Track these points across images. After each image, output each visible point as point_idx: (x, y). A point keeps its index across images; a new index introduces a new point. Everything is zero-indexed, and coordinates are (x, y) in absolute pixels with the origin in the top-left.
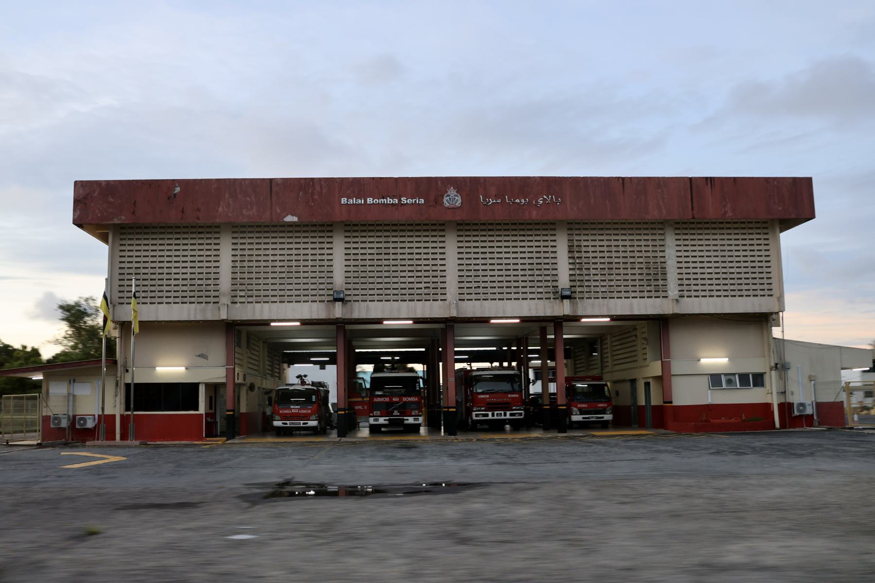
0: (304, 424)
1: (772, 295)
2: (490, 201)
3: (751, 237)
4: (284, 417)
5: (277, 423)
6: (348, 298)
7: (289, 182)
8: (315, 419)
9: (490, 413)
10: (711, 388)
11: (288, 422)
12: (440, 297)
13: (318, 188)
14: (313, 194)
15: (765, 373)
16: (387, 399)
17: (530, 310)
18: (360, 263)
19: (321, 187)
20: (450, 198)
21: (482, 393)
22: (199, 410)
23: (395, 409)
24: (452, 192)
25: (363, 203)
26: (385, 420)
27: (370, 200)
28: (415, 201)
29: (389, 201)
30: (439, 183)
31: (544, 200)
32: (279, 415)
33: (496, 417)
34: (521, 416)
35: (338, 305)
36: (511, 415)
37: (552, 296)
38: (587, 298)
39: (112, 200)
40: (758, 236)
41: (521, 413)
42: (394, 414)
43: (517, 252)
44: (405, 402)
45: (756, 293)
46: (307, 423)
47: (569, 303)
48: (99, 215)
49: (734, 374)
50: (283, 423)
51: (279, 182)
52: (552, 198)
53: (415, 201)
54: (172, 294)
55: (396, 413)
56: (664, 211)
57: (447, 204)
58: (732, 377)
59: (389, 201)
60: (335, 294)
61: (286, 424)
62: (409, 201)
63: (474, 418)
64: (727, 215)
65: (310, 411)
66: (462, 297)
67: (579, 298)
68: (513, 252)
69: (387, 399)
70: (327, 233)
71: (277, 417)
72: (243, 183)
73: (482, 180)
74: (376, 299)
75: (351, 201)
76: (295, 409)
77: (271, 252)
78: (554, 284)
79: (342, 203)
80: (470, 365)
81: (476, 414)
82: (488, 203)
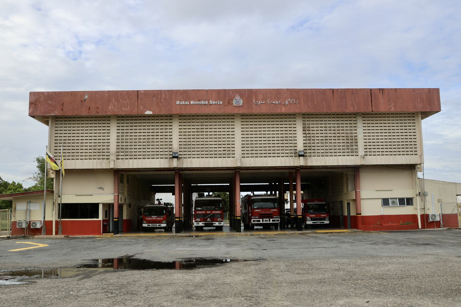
0: (159, 225)
4: (148, 222)
5: (145, 225)
7: (147, 93)
9: (261, 220)
11: (150, 224)
13: (164, 96)
14: (161, 99)
15: (413, 198)
16: (204, 212)
17: (281, 163)
19: (165, 94)
20: (236, 101)
24: (238, 98)
25: (188, 104)
26: (202, 224)
27: (192, 102)
28: (217, 103)
32: (146, 220)
33: (264, 222)
34: (279, 221)
35: (175, 160)
36: (273, 221)
38: (313, 156)
39: (50, 102)
41: (279, 220)
42: (208, 220)
44: (214, 214)
47: (303, 159)
49: (396, 198)
50: (148, 225)
51: (142, 92)
55: (209, 220)
56: (356, 108)
58: (395, 200)
61: (150, 225)
63: (252, 222)
64: (391, 110)
65: (162, 219)
66: (244, 155)
67: (309, 156)
69: (204, 212)
71: (145, 222)
72: (122, 93)
74: (259, 156)
75: (182, 103)
76: (154, 217)
77: (159, 131)
78: (295, 148)
79: (177, 104)
80: (253, 193)
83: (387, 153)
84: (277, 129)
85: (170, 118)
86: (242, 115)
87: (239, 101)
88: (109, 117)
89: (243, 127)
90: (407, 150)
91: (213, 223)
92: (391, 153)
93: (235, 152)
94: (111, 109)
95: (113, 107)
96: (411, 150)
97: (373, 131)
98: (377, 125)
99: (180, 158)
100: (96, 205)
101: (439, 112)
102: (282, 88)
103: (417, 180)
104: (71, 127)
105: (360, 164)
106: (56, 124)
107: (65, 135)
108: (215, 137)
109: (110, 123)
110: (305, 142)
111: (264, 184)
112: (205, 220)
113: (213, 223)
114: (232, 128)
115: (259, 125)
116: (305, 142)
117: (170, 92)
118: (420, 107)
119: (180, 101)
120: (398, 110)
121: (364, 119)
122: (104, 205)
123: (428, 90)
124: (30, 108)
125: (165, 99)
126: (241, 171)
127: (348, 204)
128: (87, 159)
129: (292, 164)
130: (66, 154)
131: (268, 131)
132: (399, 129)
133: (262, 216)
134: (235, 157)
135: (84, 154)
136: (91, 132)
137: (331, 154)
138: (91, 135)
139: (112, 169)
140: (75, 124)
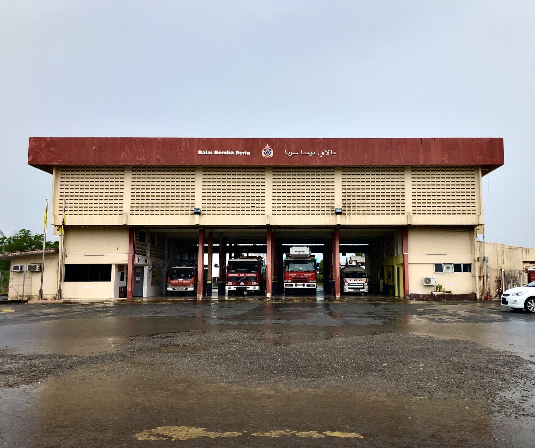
0: (185, 289)
1: (475, 214)
2: (291, 154)
3: (294, 177)
4: (175, 285)
5: (170, 289)
6: (202, 212)
7: (165, 140)
8: (192, 286)
9: (294, 284)
10: (435, 272)
11: (176, 288)
12: (401, 212)
13: (184, 144)
14: (180, 148)
15: (472, 263)
18: (185, 191)
19: (186, 143)
20: (266, 152)
21: (292, 272)
22: (111, 280)
23: (242, 281)
24: (268, 147)
25: (212, 154)
26: (235, 288)
27: (216, 152)
28: (245, 153)
29: (228, 153)
30: (260, 142)
31: (326, 153)
32: (171, 284)
33: (298, 287)
34: (314, 286)
35: (197, 216)
36: (308, 286)
37: (190, 212)
39: (53, 150)
40: (468, 176)
42: (241, 284)
43: (250, 186)
44: (247, 277)
45: (435, 212)
46: (187, 289)
48: (45, 159)
49: (451, 264)
50: (173, 289)
51: (160, 140)
52: (330, 152)
53: (245, 153)
54: (93, 209)
55: (242, 283)
56: (403, 160)
57: (264, 155)
58: (449, 266)
59: (228, 153)
60: (195, 210)
61: (175, 289)
62: (241, 153)
63: (285, 287)
64: (444, 162)
65: (189, 282)
66: (274, 212)
68: (288, 186)
70: (436, 172)
71: (170, 285)
72: (137, 140)
73: (287, 141)
74: (432, 213)
75: (204, 153)
76: (181, 280)
77: (181, 184)
78: (332, 205)
79: (199, 153)
81: (286, 285)
82: (289, 155)
83: (439, 212)
84: (303, 184)
85: (263, 170)
86: (412, 167)
87: (269, 152)
88: (264, 168)
89: (275, 180)
90: (463, 208)
91: (246, 288)
92: (444, 212)
93: (405, 209)
94: (123, 157)
95: (126, 157)
96: (468, 208)
97: (313, 187)
98: (428, 180)
99: (203, 214)
100: (109, 266)
101: (503, 164)
102: (318, 137)
103: (476, 244)
104: (69, 178)
105: (407, 224)
106: (62, 174)
107: (72, 187)
108: (229, 191)
109: (124, 174)
110: (343, 198)
111: (318, 245)
112: (238, 284)
113: (246, 288)
114: (247, 182)
115: (262, 179)
116: (343, 198)
117: (191, 141)
118: (479, 160)
119: (203, 150)
120: (453, 163)
121: (413, 173)
122: (116, 265)
123: (489, 139)
124: (29, 156)
125: (185, 148)
126: (341, 230)
127: (398, 268)
128: (97, 214)
129: (333, 223)
130: (331, 205)
131: (307, 186)
132: (235, 186)
133: (296, 280)
134: (264, 214)
135: (93, 209)
136: (153, 183)
137: (373, 212)
138: (102, 187)
139: (125, 225)
140: (140, 174)
